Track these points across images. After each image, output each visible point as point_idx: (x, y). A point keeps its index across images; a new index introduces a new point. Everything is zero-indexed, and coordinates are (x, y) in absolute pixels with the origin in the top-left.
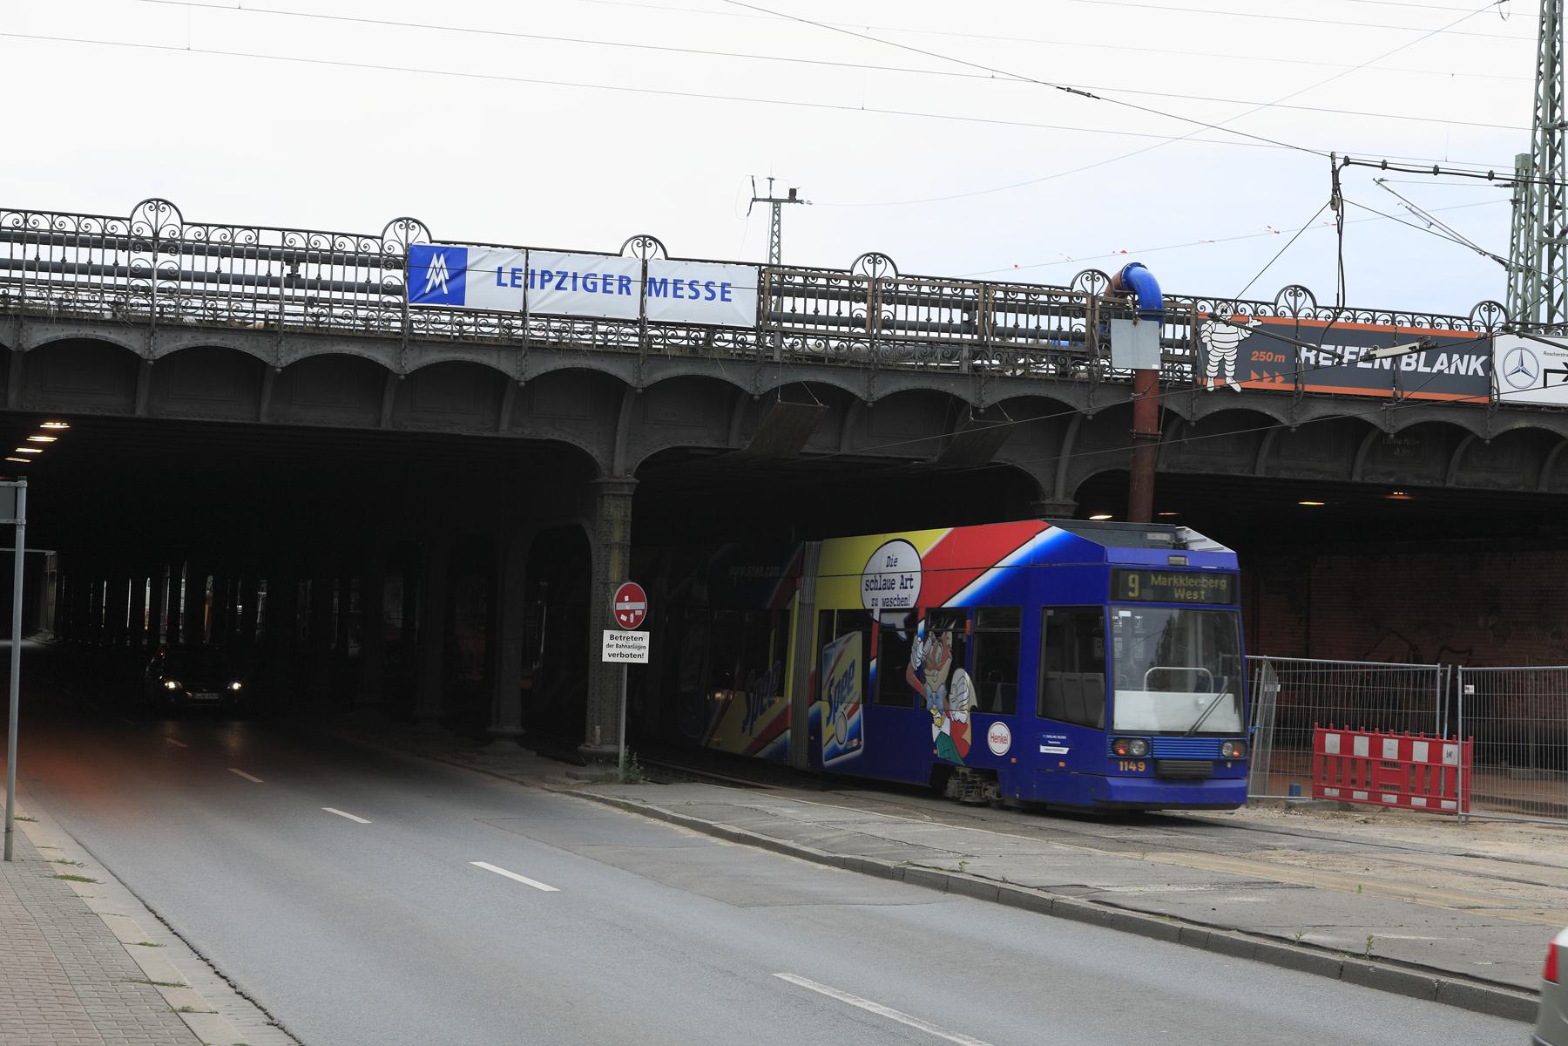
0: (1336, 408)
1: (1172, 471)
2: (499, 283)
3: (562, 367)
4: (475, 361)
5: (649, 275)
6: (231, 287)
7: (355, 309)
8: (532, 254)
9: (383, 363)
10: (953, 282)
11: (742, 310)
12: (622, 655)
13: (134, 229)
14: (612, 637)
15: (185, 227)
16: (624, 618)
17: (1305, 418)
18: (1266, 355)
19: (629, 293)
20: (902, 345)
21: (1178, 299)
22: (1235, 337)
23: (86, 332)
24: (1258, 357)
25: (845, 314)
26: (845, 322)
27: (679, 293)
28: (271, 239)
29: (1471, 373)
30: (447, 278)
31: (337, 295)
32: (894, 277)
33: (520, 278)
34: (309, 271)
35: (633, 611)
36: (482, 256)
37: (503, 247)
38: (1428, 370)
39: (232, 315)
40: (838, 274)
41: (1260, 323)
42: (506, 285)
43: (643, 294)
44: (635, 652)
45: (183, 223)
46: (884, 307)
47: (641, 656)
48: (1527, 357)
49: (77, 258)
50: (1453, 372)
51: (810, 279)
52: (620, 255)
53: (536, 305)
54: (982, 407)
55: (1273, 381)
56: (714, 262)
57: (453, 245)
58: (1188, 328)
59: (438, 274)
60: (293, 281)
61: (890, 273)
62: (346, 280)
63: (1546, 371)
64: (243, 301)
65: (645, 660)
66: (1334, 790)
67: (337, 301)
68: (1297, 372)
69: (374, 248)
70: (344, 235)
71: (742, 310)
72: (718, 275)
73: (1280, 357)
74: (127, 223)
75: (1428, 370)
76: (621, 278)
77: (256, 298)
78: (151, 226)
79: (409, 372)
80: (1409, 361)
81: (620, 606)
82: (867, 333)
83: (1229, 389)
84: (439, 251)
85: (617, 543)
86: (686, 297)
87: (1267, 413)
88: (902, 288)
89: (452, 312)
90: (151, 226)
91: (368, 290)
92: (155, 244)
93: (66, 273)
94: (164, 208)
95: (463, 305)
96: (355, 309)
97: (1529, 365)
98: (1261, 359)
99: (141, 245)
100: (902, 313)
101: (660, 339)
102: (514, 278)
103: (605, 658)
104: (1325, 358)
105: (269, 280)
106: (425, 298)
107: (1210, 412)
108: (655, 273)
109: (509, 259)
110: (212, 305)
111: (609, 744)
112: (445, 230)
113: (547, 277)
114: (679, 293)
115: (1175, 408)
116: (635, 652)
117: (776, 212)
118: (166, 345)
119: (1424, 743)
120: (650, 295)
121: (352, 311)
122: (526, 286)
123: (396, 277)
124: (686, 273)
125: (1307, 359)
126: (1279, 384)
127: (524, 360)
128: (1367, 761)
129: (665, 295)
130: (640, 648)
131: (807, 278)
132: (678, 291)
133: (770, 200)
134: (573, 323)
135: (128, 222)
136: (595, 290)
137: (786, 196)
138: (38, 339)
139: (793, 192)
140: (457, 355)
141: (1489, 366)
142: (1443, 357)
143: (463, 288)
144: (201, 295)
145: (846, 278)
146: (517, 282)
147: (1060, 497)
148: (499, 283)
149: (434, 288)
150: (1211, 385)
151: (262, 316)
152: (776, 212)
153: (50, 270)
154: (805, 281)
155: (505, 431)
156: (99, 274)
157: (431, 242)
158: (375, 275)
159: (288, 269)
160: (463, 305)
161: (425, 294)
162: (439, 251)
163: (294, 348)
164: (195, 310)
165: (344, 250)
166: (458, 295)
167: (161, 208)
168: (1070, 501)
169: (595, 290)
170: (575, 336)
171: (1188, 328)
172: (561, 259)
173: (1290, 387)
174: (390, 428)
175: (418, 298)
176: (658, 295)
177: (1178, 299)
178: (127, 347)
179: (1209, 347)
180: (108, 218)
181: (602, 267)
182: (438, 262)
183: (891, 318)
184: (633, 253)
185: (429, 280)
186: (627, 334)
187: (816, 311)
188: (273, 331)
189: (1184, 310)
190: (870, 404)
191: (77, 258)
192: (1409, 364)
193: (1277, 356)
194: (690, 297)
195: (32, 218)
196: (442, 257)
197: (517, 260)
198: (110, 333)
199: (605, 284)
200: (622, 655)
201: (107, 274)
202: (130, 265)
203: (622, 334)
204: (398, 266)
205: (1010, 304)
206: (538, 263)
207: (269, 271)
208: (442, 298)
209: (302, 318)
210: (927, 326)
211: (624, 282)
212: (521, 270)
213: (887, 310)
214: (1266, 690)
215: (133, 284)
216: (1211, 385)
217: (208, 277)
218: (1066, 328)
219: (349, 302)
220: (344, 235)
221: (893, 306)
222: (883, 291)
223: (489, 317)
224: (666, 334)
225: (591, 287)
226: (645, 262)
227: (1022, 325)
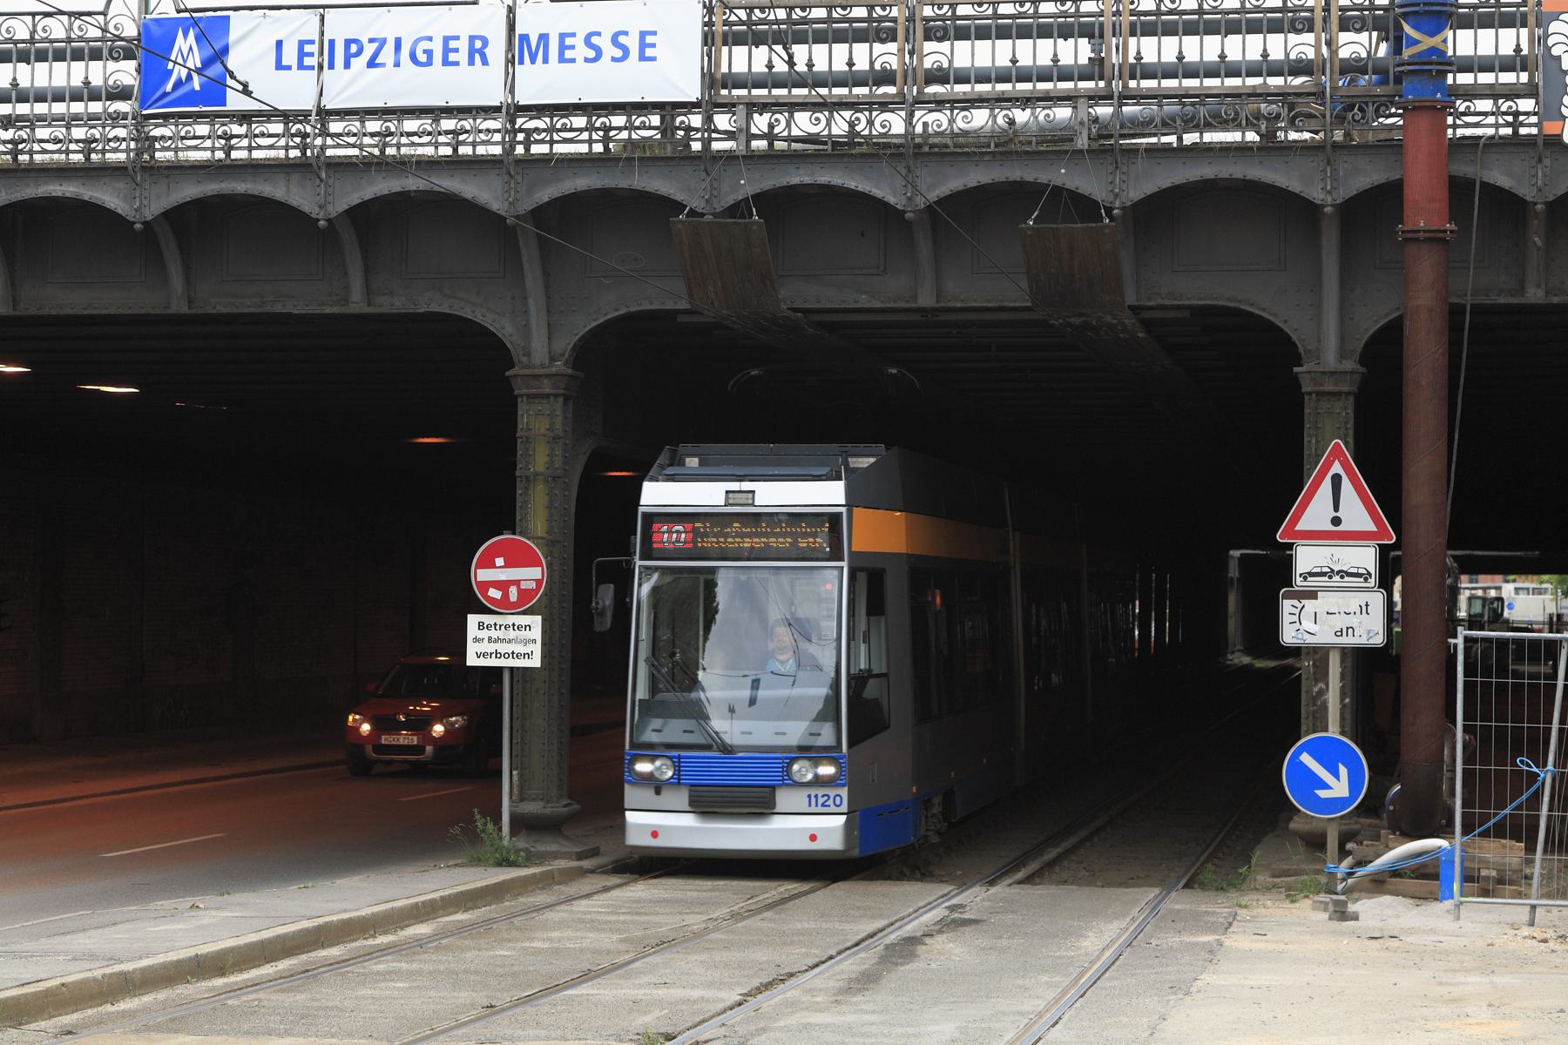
1: (1555, 300)
2: (279, 66)
4: (250, 192)
5: (519, 30)
6: (32, 110)
7: (68, 127)
12: (498, 655)
14: (481, 626)
16: (494, 593)
19: (485, 62)
20: (1193, 104)
23: (413, 183)
27: (568, 54)
30: (199, 65)
31: (41, 108)
33: (311, 55)
35: (517, 583)
36: (254, 24)
42: (289, 68)
43: (510, 61)
46: (929, 46)
47: (528, 655)
51: (798, 10)
53: (339, 94)
54: (1117, 204)
56: (289, 8)
59: (186, 51)
65: (535, 662)
67: (41, 118)
74: (101, 18)
76: (472, 39)
81: (483, 575)
82: (901, 93)
85: (540, 474)
86: (580, 60)
89: (211, 117)
91: (1223, 73)
95: (225, 105)
96: (68, 127)
100: (1150, 49)
102: (302, 54)
103: (472, 660)
110: (1510, 107)
111: (534, 799)
113: (354, 48)
114: (568, 54)
116: (519, 649)
122: (321, 67)
123: (125, 73)
127: (1539, 166)
129: (546, 61)
130: (526, 642)
132: (566, 52)
134: (436, 121)
136: (429, 63)
140: (223, 185)
144: (1494, 93)
146: (307, 61)
147: (1330, 359)
148: (279, 66)
154: (870, 13)
155: (357, 303)
156: (1471, 71)
158: (96, 73)
160: (225, 105)
161: (165, 94)
165: (122, 35)
169: (429, 63)
170: (404, 140)
171: (1524, 32)
176: (533, 61)
194: (587, 60)
196: (191, 34)
198: (61, 185)
200: (498, 655)
201: (1504, 69)
202: (1287, 55)
204: (129, 55)
205: (1506, 13)
207: (1223, 50)
210: (1224, 68)
212: (312, 42)
213: (935, 54)
215: (111, 110)
221: (948, 43)
222: (927, 20)
225: (422, 58)
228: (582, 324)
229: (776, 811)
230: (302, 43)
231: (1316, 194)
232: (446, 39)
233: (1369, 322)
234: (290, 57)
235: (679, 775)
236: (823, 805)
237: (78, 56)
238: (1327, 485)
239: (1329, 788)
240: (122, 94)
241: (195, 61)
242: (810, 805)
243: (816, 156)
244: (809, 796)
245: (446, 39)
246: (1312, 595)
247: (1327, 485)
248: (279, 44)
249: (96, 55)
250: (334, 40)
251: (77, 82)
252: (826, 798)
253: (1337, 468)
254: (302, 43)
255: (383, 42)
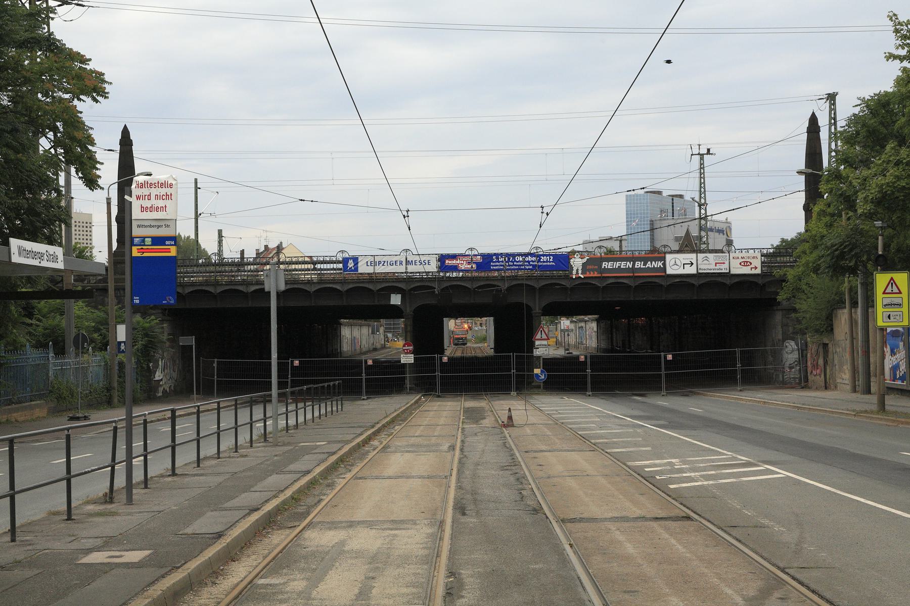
2: (367, 266)
5: (408, 260)
11: (433, 267)
16: (406, 351)
19: (402, 265)
29: (658, 267)
34: (318, 266)
38: (644, 267)
43: (406, 265)
44: (410, 360)
48: (677, 261)
50: (652, 267)
55: (594, 274)
59: (351, 264)
60: (315, 269)
63: (684, 264)
65: (413, 362)
69: (334, 259)
71: (433, 267)
72: (426, 258)
75: (644, 267)
97: (678, 262)
102: (371, 264)
108: (409, 259)
112: (352, 253)
116: (410, 360)
117: (702, 159)
123: (340, 266)
125: (605, 267)
126: (596, 275)
133: (699, 154)
137: (706, 152)
139: (709, 150)
141: (664, 264)
142: (649, 262)
143: (358, 267)
148: (367, 266)
149: (350, 268)
150: (574, 277)
152: (702, 159)
158: (335, 266)
159: (316, 267)
162: (351, 258)
166: (356, 269)
168: (540, 311)
173: (600, 275)
181: (394, 259)
182: (351, 261)
184: (404, 254)
188: (310, 282)
192: (638, 266)
195: (249, 259)
197: (372, 259)
199: (396, 263)
206: (377, 259)
216: (574, 277)
228: (415, 306)
230: (371, 262)
231: (536, 286)
232: (396, 261)
234: (369, 264)
237: (332, 263)
238: (540, 331)
240: (340, 269)
241: (353, 265)
243: (420, 281)
245: (396, 261)
246: (538, 348)
247: (540, 331)
248: (367, 262)
249: (335, 263)
250: (222, 230)
251: (332, 267)
253: (541, 329)
254: (371, 262)
255: (385, 262)
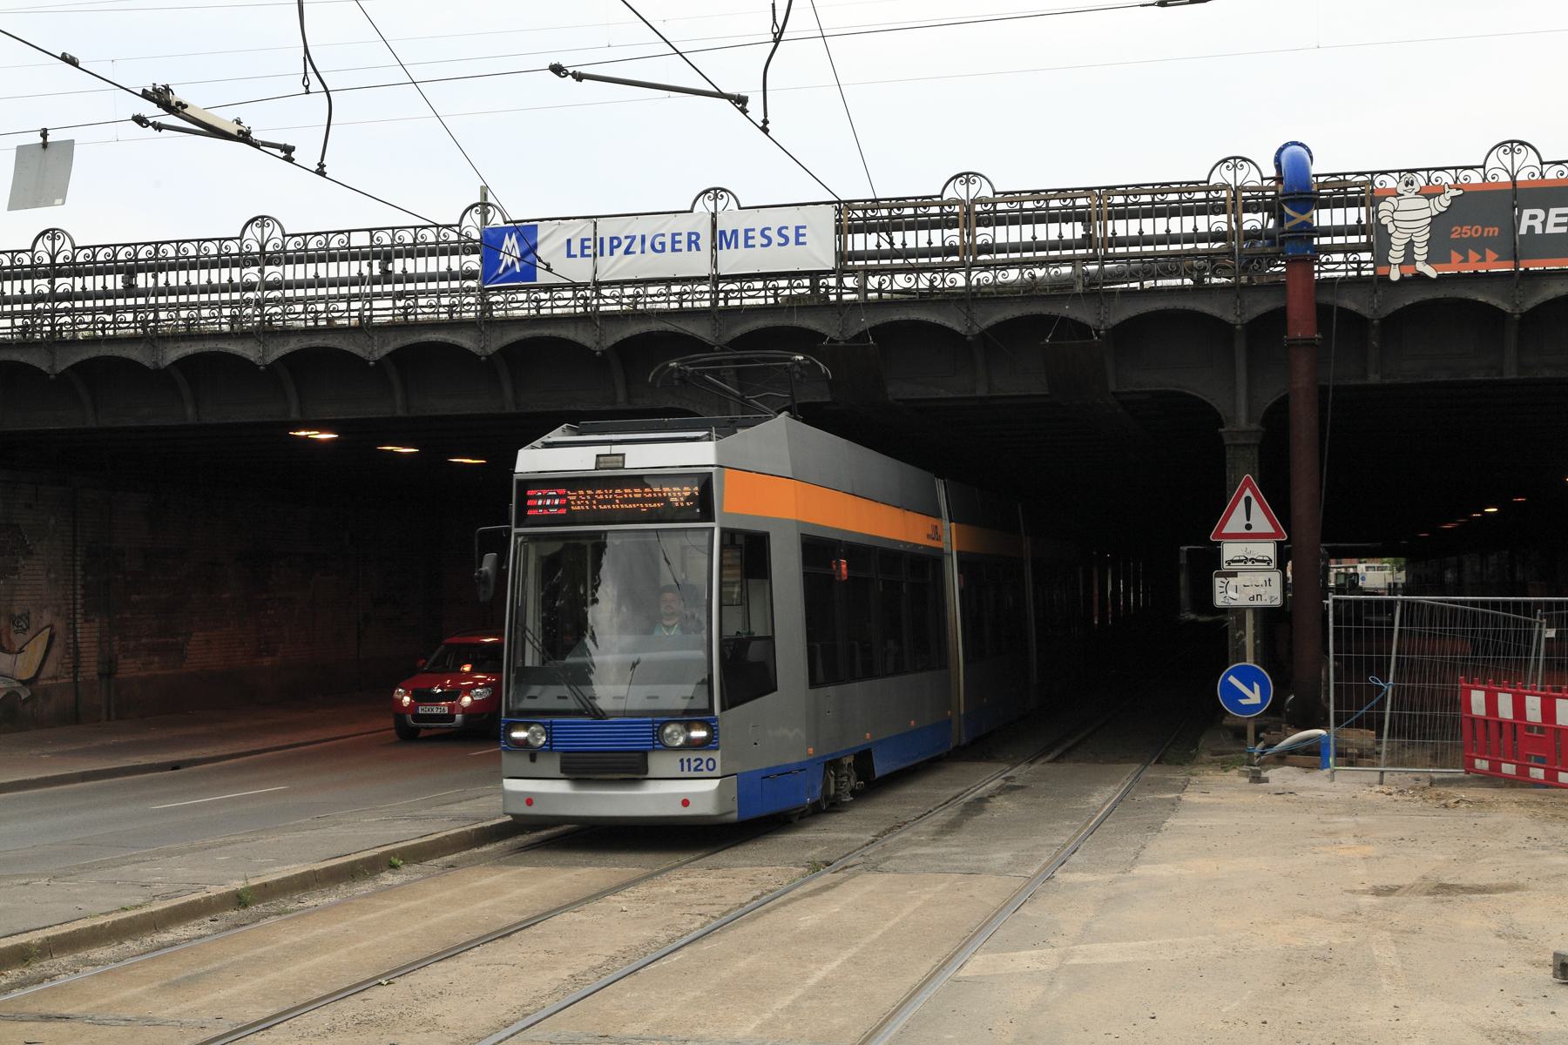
0: (191, 346)
2: (569, 255)
3: (638, 333)
8: (600, 222)
9: (467, 346)
10: (1061, 193)
11: (819, 252)
13: (1489, 177)
15: (1546, 167)
17: (1530, 304)
18: (1471, 230)
19: (698, 249)
21: (1348, 177)
22: (1427, 213)
23: (210, 346)
24: (1460, 233)
25: (28, 291)
26: (235, 288)
27: (750, 242)
28: (360, 240)
32: (991, 195)
33: (589, 247)
37: (574, 218)
39: (330, 316)
40: (926, 201)
41: (1460, 192)
42: (575, 256)
43: (714, 247)
45: (1542, 163)
49: (12, 285)
52: (691, 211)
57: (525, 224)
58: (1363, 210)
61: (987, 192)
62: (1184, 232)
64: (338, 301)
66: (1484, 761)
67: (421, 292)
68: (1516, 247)
70: (1383, 173)
72: (791, 218)
73: (1491, 229)
77: (349, 298)
78: (1507, 171)
79: (491, 353)
80: (1532, 222)
82: (962, 260)
83: (1420, 277)
84: (510, 231)
86: (758, 246)
87: (1480, 300)
88: (1000, 206)
89: (528, 289)
90: (1507, 171)
92: (264, 258)
93: (396, 283)
94: (1519, 150)
98: (1464, 236)
99: (243, 260)
100: (1121, 228)
101: (736, 293)
102: (583, 248)
104: (1489, 231)
105: (449, 275)
106: (499, 279)
107: (1399, 306)
109: (578, 230)
112: (519, 210)
113: (615, 243)
114: (750, 242)
115: (1352, 306)
118: (278, 350)
119: (707, 703)
120: (721, 248)
121: (436, 299)
122: (595, 255)
123: (473, 262)
124: (757, 221)
128: (1541, 729)
129: (736, 247)
131: (866, 210)
135: (1482, 169)
136: (663, 250)
138: (172, 356)
145: (935, 204)
146: (587, 252)
148: (569, 255)
149: (507, 268)
151: (356, 314)
153: (1168, 242)
154: (941, 210)
157: (505, 223)
158: (455, 263)
161: (499, 275)
162: (510, 231)
163: (386, 341)
164: (298, 317)
165: (230, 252)
167: (1516, 150)
169: (663, 250)
170: (648, 299)
171: (1363, 210)
172: (629, 224)
174: (514, 410)
175: (492, 280)
176: (728, 247)
177: (1348, 177)
178: (244, 356)
179: (1391, 229)
180: (1431, 169)
181: (670, 225)
182: (510, 243)
183: (281, 279)
184: (705, 207)
185: (502, 260)
186: (701, 292)
187: (22, 291)
188: (365, 327)
189: (1358, 189)
190: (969, 338)
191: (12, 285)
193: (1487, 229)
194: (762, 245)
195: (1378, 179)
196: (514, 237)
197: (585, 230)
203: (696, 293)
204: (475, 251)
206: (607, 230)
208: (515, 277)
209: (390, 312)
211: (694, 238)
212: (589, 240)
213: (983, 235)
214: (1547, 636)
217: (1010, 249)
218: (236, 280)
219: (433, 292)
220: (1383, 173)
221: (71, 278)
223: (563, 290)
224: (742, 288)
225: (659, 247)
226: (714, 215)
227: (89, 287)
229: (648, 776)
233: (1268, 399)
235: (551, 742)
236: (696, 769)
239: (1247, 697)
240: (471, 275)
242: (682, 770)
244: (682, 761)
252: (699, 762)
